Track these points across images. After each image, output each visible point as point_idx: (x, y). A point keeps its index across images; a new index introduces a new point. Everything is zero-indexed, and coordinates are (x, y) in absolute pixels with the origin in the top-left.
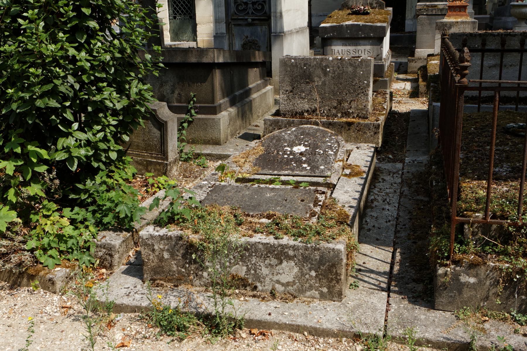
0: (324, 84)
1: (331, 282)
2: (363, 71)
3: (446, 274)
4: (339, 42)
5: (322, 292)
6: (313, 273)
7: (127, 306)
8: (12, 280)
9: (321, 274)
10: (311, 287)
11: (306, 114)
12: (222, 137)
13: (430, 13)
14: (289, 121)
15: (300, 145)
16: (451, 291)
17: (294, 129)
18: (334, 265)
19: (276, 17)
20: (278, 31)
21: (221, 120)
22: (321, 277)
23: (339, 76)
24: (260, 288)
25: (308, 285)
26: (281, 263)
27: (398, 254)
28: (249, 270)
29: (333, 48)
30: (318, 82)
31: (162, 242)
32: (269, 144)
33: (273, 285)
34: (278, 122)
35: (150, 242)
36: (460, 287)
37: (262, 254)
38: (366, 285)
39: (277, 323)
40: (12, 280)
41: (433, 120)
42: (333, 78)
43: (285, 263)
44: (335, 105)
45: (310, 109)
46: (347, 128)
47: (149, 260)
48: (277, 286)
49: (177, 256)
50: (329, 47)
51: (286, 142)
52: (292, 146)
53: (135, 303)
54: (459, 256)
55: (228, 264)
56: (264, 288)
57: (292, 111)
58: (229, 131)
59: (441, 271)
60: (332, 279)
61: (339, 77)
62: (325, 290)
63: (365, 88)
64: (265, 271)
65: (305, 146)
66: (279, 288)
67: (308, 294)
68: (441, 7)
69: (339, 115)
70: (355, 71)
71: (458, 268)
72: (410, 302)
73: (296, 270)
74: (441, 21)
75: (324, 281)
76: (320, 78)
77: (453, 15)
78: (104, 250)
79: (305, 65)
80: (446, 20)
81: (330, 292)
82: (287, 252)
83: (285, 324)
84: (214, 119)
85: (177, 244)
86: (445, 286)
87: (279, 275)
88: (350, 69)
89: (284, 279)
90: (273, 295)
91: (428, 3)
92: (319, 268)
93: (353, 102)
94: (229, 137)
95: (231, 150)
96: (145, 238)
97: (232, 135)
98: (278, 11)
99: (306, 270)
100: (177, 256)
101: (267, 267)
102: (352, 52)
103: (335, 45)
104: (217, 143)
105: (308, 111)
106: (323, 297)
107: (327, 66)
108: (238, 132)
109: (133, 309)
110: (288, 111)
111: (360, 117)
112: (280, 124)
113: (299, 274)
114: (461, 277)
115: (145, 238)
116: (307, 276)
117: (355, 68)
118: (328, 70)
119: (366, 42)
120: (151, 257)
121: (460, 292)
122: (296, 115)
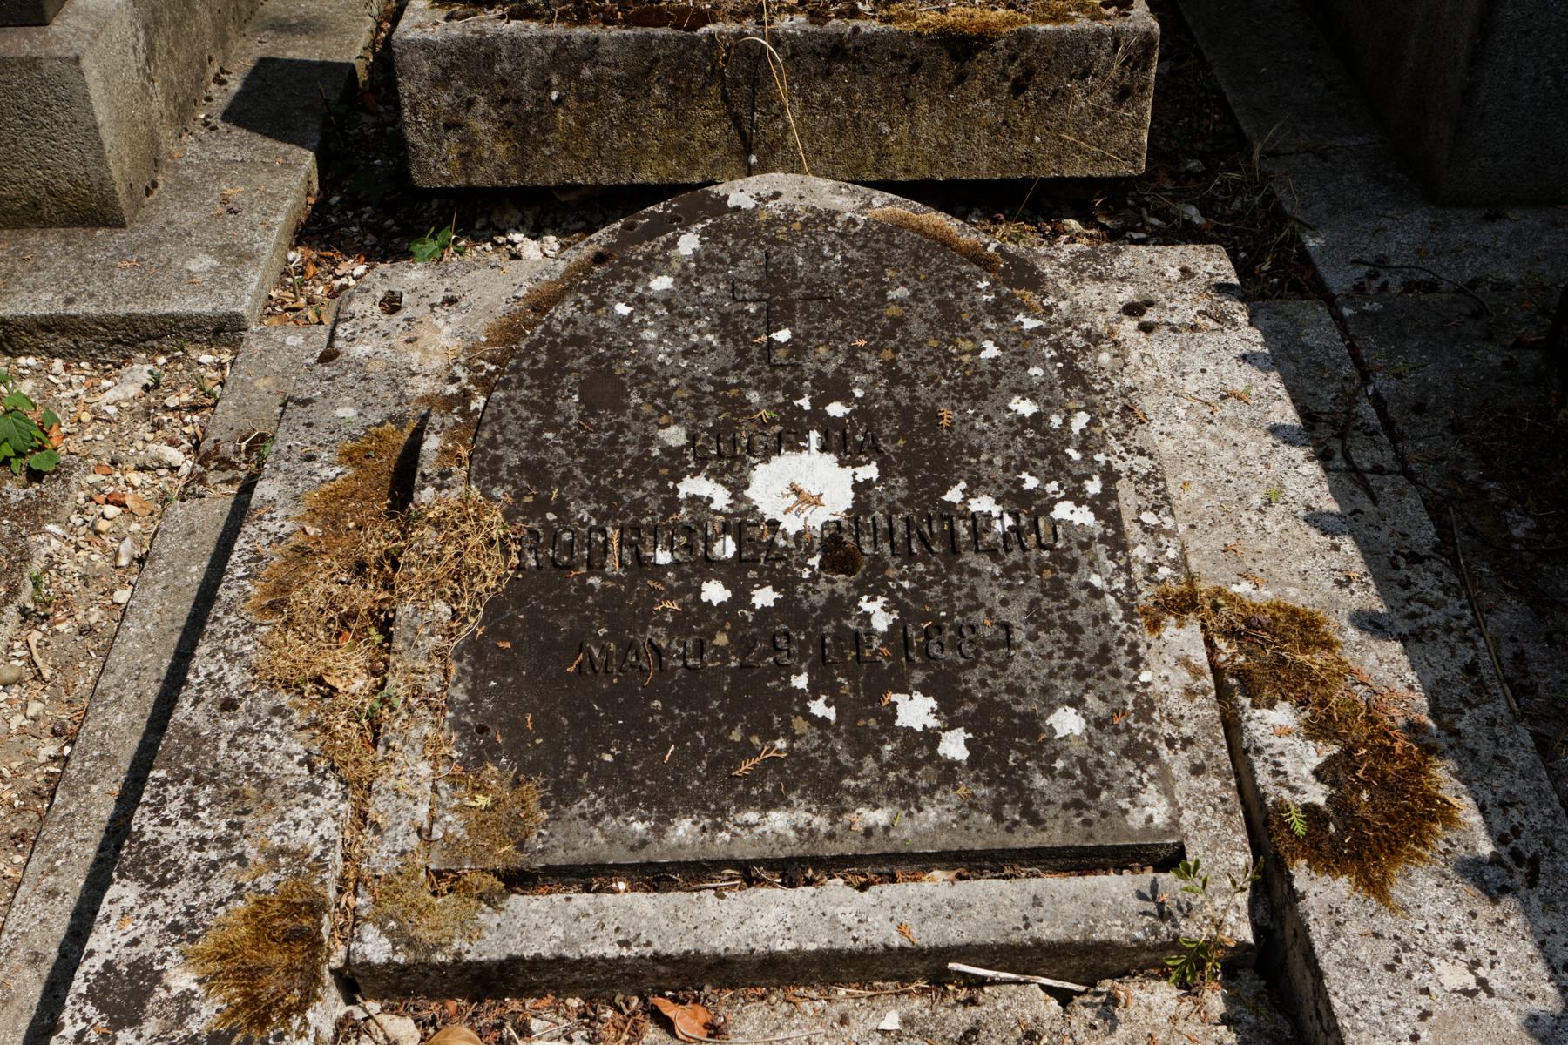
12: (120, 163)
14: (563, 44)
17: (688, 244)
21: (86, 63)
32: (536, 444)
34: (490, 57)
46: (948, 71)
52: (729, 459)
58: (158, 103)
65: (841, 444)
84: (32, 63)
94: (166, 135)
95: (201, 263)
97: (181, 114)
104: (91, 212)
108: (214, 69)
112: (504, 67)
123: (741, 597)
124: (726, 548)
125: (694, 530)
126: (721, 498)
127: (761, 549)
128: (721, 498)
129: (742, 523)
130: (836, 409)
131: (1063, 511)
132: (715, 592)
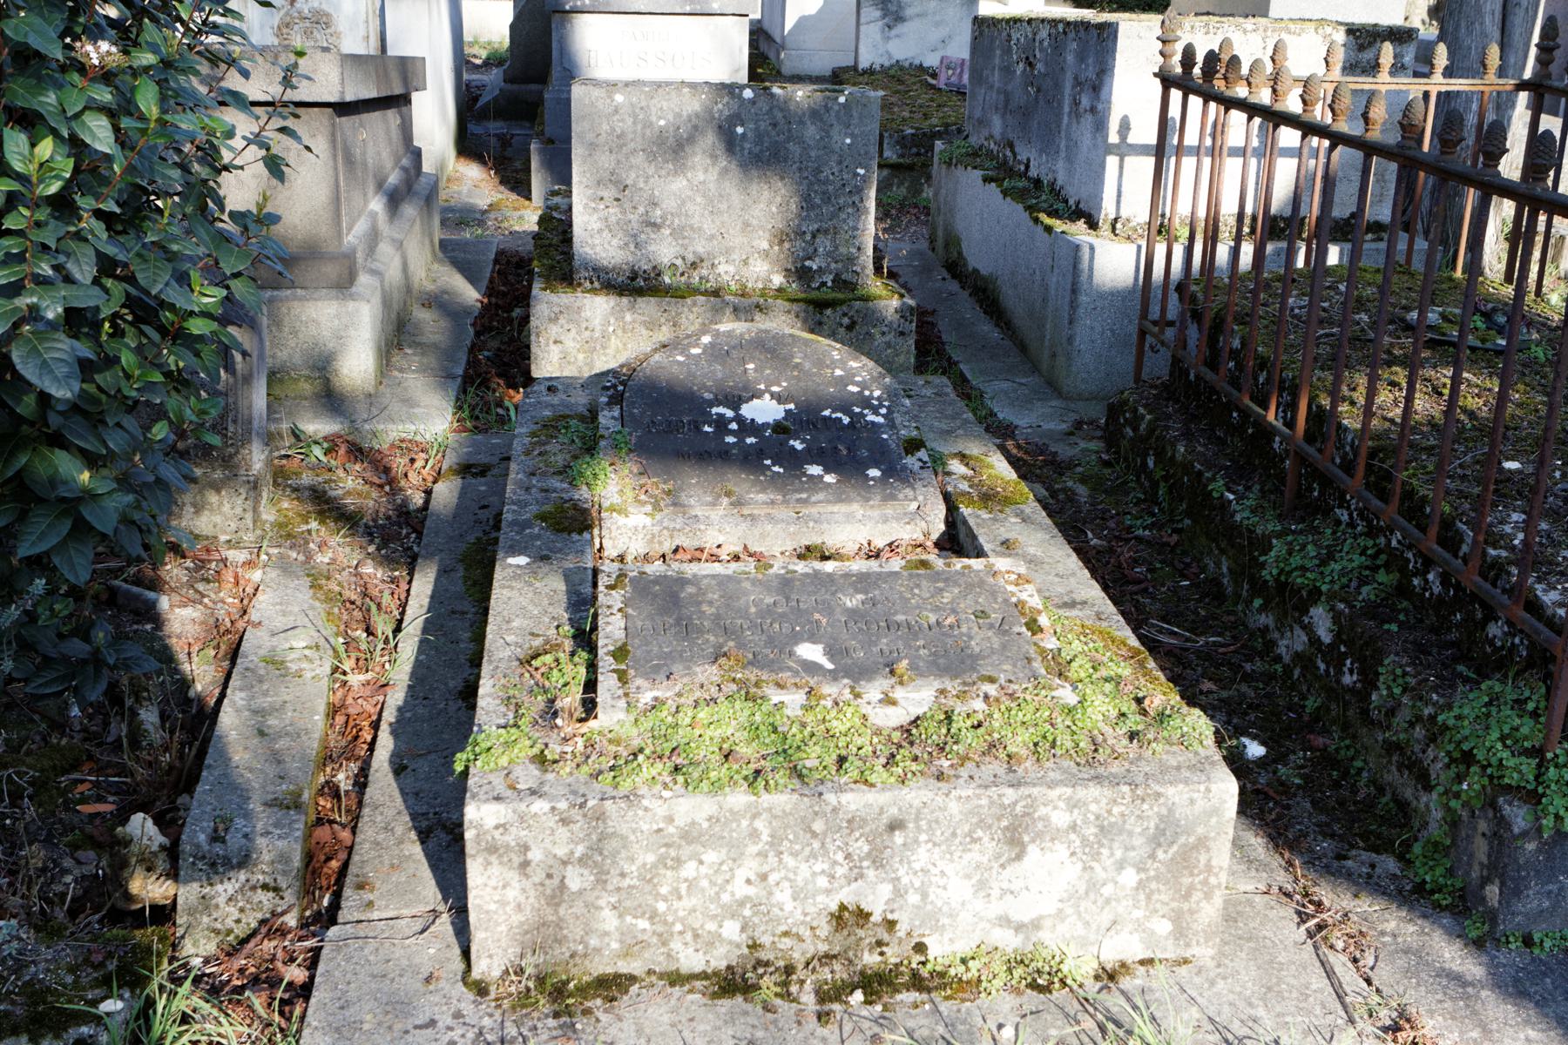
2: (852, 136)
5: (1153, 933)
9: (1157, 878)
22: (1154, 885)
35: (510, 839)
37: (954, 834)
41: (336, 169)
45: (679, 262)
87: (1009, 897)
92: (1153, 856)
99: (1104, 869)
118: (740, 130)
123: (741, 440)
124: (734, 426)
125: (721, 423)
126: (730, 413)
127: (748, 427)
128: (730, 413)
129: (739, 419)
130: (775, 389)
131: (871, 418)
132: (730, 439)
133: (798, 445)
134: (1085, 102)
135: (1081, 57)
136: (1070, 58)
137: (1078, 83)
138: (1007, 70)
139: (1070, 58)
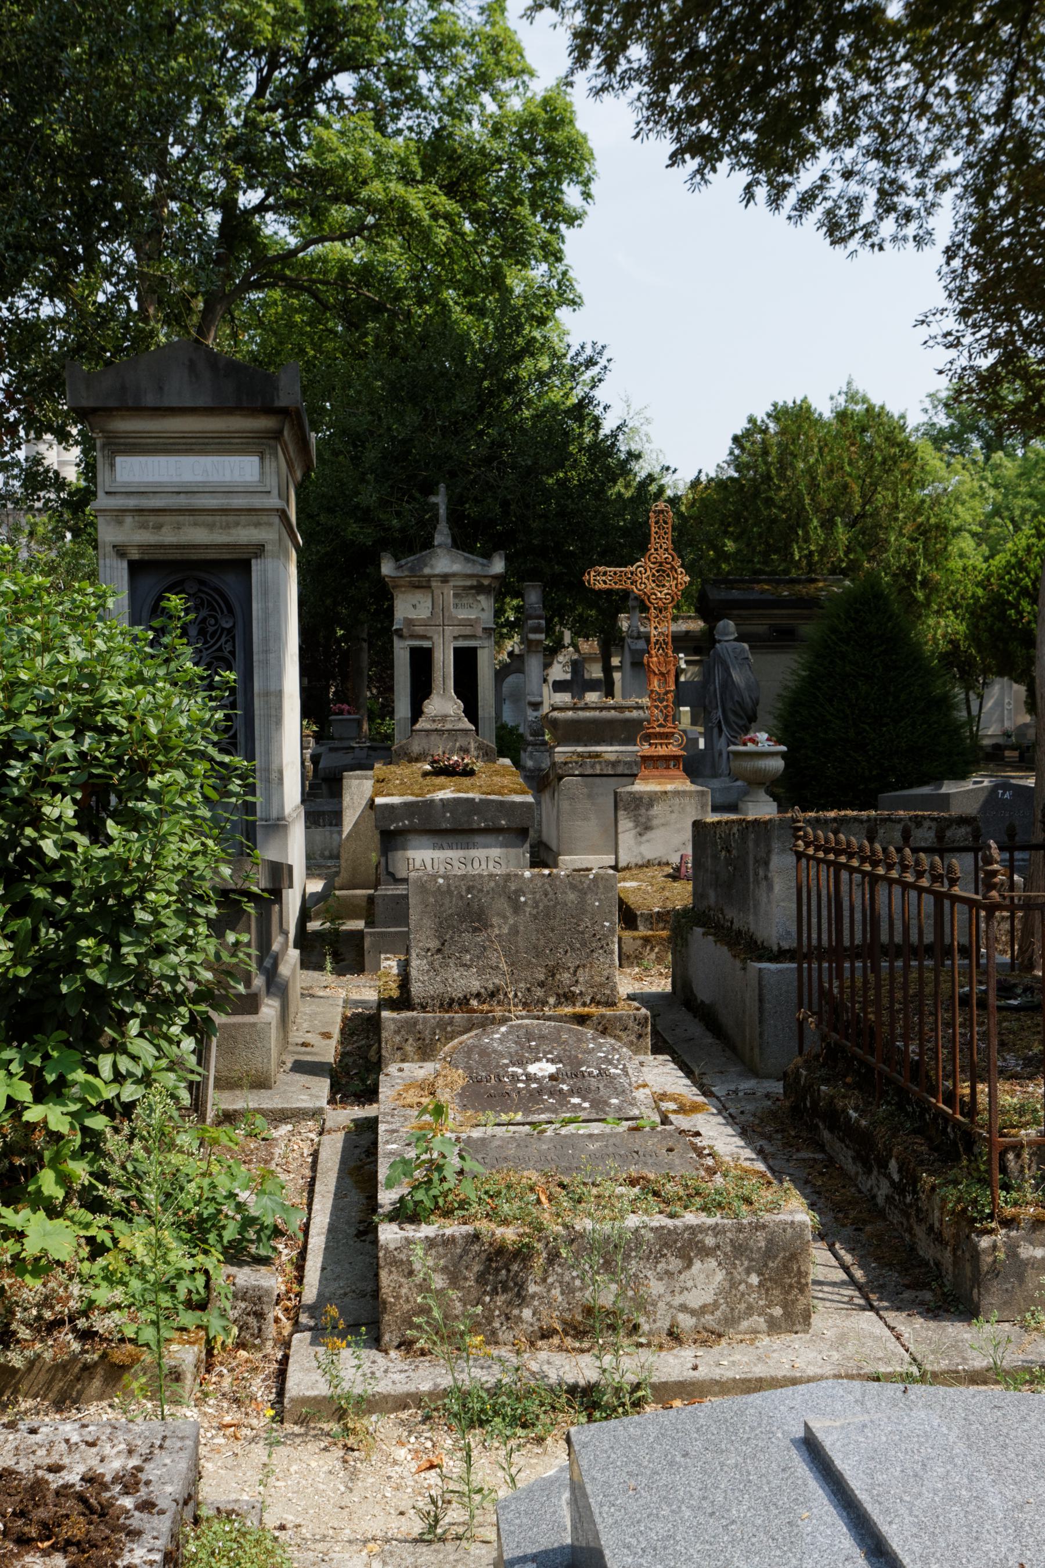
0: (514, 931)
1: (788, 1293)
3: (995, 1247)
4: (424, 840)
5: (772, 1316)
6: (754, 1279)
7: (385, 1398)
8: (56, 1389)
9: (770, 1279)
10: (750, 1310)
11: (474, 1003)
13: (589, 772)
15: (539, 1060)
16: (1006, 1279)
18: (793, 1257)
19: (268, 781)
20: (274, 814)
23: (548, 914)
24: (645, 1327)
25: (743, 1306)
26: (689, 1266)
27: (842, 1252)
28: (623, 1290)
29: (411, 854)
30: (500, 927)
31: (433, 1252)
33: (673, 1317)
34: (415, 1024)
35: (403, 1257)
36: (1019, 1268)
38: (828, 1304)
39: (717, 1382)
40: (56, 1389)
42: (535, 917)
43: (697, 1265)
44: (542, 977)
47: (397, 1297)
48: (681, 1317)
49: (466, 1279)
50: (400, 854)
51: (503, 1057)
53: (402, 1388)
54: (1009, 1211)
55: (578, 1283)
56: (654, 1326)
57: (441, 997)
59: (985, 1242)
60: (791, 1286)
61: (547, 915)
62: (777, 1311)
63: (606, 937)
64: (656, 1287)
65: (552, 1061)
66: (686, 1321)
67: (745, 1324)
68: (612, 757)
69: (552, 1000)
70: (582, 901)
71: (1013, 1233)
72: (926, 1318)
73: (720, 1276)
74: (629, 789)
75: (776, 1292)
76: (505, 917)
77: (654, 777)
78: (243, 1305)
79: (469, 890)
80: (639, 787)
81: (788, 1315)
82: (702, 1241)
83: (734, 1380)
84: (254, 1025)
85: (466, 1252)
86: (995, 1271)
88: (572, 896)
89: (696, 1299)
90: (674, 1336)
91: (580, 749)
92: (766, 1265)
93: (580, 971)
96: (392, 1247)
98: (274, 767)
100: (466, 1279)
101: (661, 1279)
102: (456, 864)
103: (415, 848)
105: (478, 995)
106: (774, 1327)
107: (519, 892)
109: (401, 1402)
110: (433, 998)
111: (598, 1003)
112: (420, 1027)
113: (727, 1285)
114: (1020, 1250)
115: (392, 1247)
116: (742, 1287)
117: (583, 893)
119: (489, 839)
120: (404, 1291)
121: (1021, 1278)
122: (450, 1005)
125: (515, 1078)
128: (520, 1071)
132: (521, 1085)
133: (565, 1087)
134: (761, 873)
135: (757, 844)
136: (751, 844)
137: (756, 861)
138: (715, 857)
139: (751, 844)
